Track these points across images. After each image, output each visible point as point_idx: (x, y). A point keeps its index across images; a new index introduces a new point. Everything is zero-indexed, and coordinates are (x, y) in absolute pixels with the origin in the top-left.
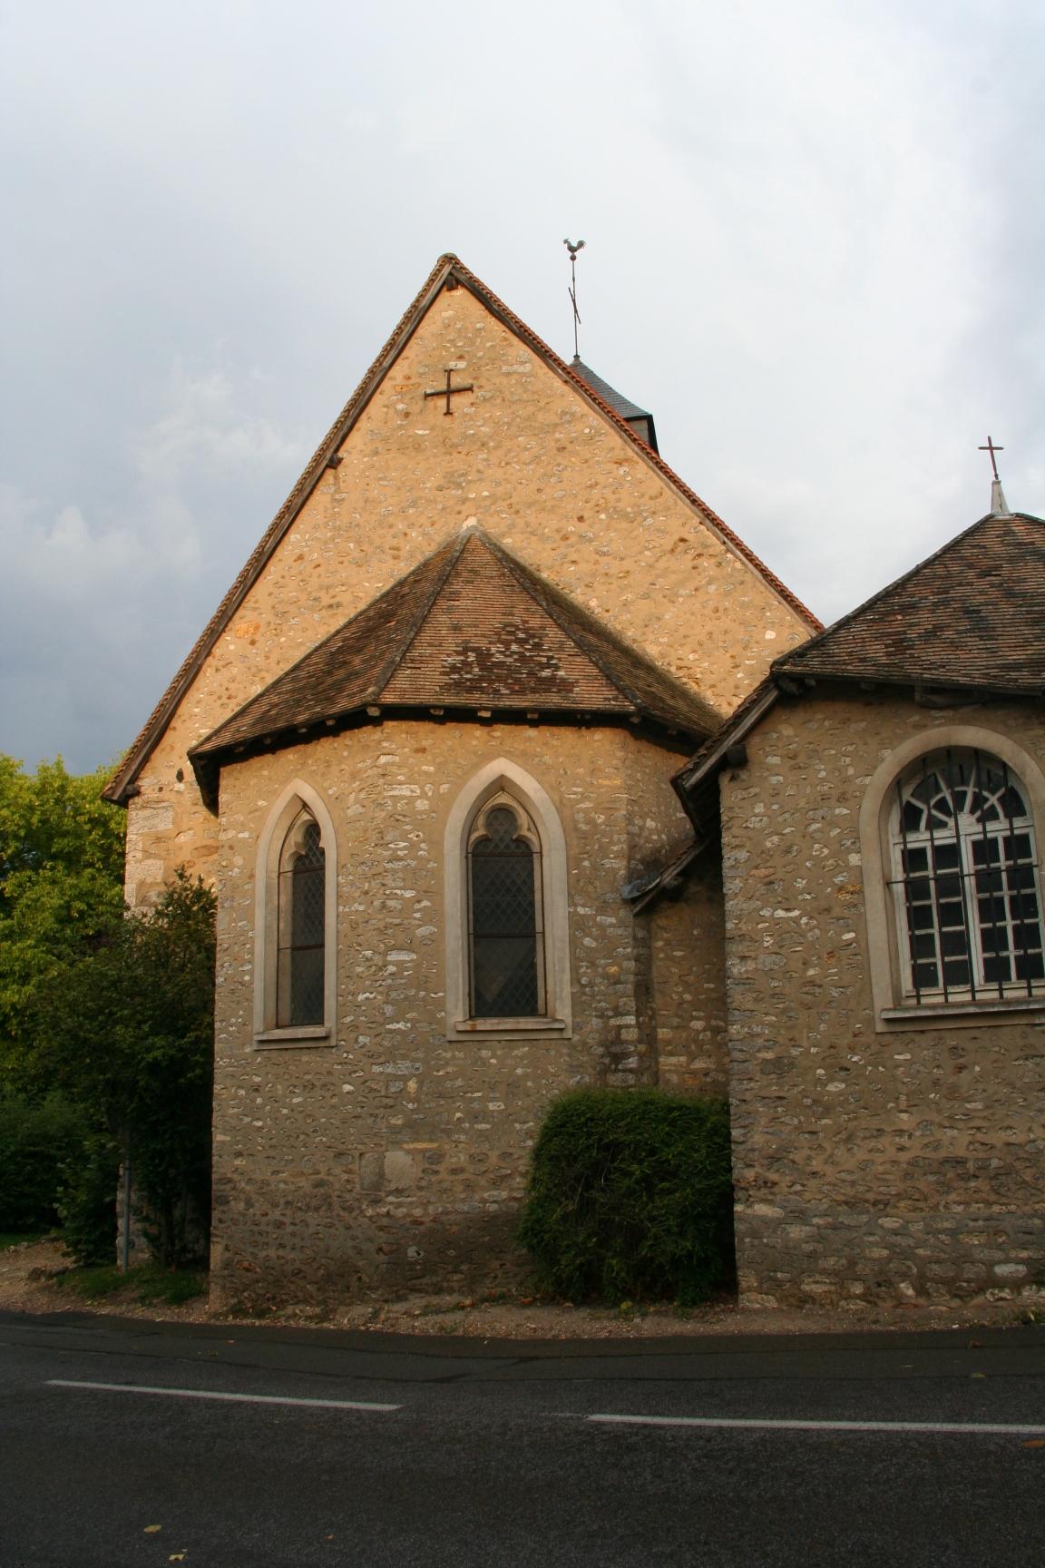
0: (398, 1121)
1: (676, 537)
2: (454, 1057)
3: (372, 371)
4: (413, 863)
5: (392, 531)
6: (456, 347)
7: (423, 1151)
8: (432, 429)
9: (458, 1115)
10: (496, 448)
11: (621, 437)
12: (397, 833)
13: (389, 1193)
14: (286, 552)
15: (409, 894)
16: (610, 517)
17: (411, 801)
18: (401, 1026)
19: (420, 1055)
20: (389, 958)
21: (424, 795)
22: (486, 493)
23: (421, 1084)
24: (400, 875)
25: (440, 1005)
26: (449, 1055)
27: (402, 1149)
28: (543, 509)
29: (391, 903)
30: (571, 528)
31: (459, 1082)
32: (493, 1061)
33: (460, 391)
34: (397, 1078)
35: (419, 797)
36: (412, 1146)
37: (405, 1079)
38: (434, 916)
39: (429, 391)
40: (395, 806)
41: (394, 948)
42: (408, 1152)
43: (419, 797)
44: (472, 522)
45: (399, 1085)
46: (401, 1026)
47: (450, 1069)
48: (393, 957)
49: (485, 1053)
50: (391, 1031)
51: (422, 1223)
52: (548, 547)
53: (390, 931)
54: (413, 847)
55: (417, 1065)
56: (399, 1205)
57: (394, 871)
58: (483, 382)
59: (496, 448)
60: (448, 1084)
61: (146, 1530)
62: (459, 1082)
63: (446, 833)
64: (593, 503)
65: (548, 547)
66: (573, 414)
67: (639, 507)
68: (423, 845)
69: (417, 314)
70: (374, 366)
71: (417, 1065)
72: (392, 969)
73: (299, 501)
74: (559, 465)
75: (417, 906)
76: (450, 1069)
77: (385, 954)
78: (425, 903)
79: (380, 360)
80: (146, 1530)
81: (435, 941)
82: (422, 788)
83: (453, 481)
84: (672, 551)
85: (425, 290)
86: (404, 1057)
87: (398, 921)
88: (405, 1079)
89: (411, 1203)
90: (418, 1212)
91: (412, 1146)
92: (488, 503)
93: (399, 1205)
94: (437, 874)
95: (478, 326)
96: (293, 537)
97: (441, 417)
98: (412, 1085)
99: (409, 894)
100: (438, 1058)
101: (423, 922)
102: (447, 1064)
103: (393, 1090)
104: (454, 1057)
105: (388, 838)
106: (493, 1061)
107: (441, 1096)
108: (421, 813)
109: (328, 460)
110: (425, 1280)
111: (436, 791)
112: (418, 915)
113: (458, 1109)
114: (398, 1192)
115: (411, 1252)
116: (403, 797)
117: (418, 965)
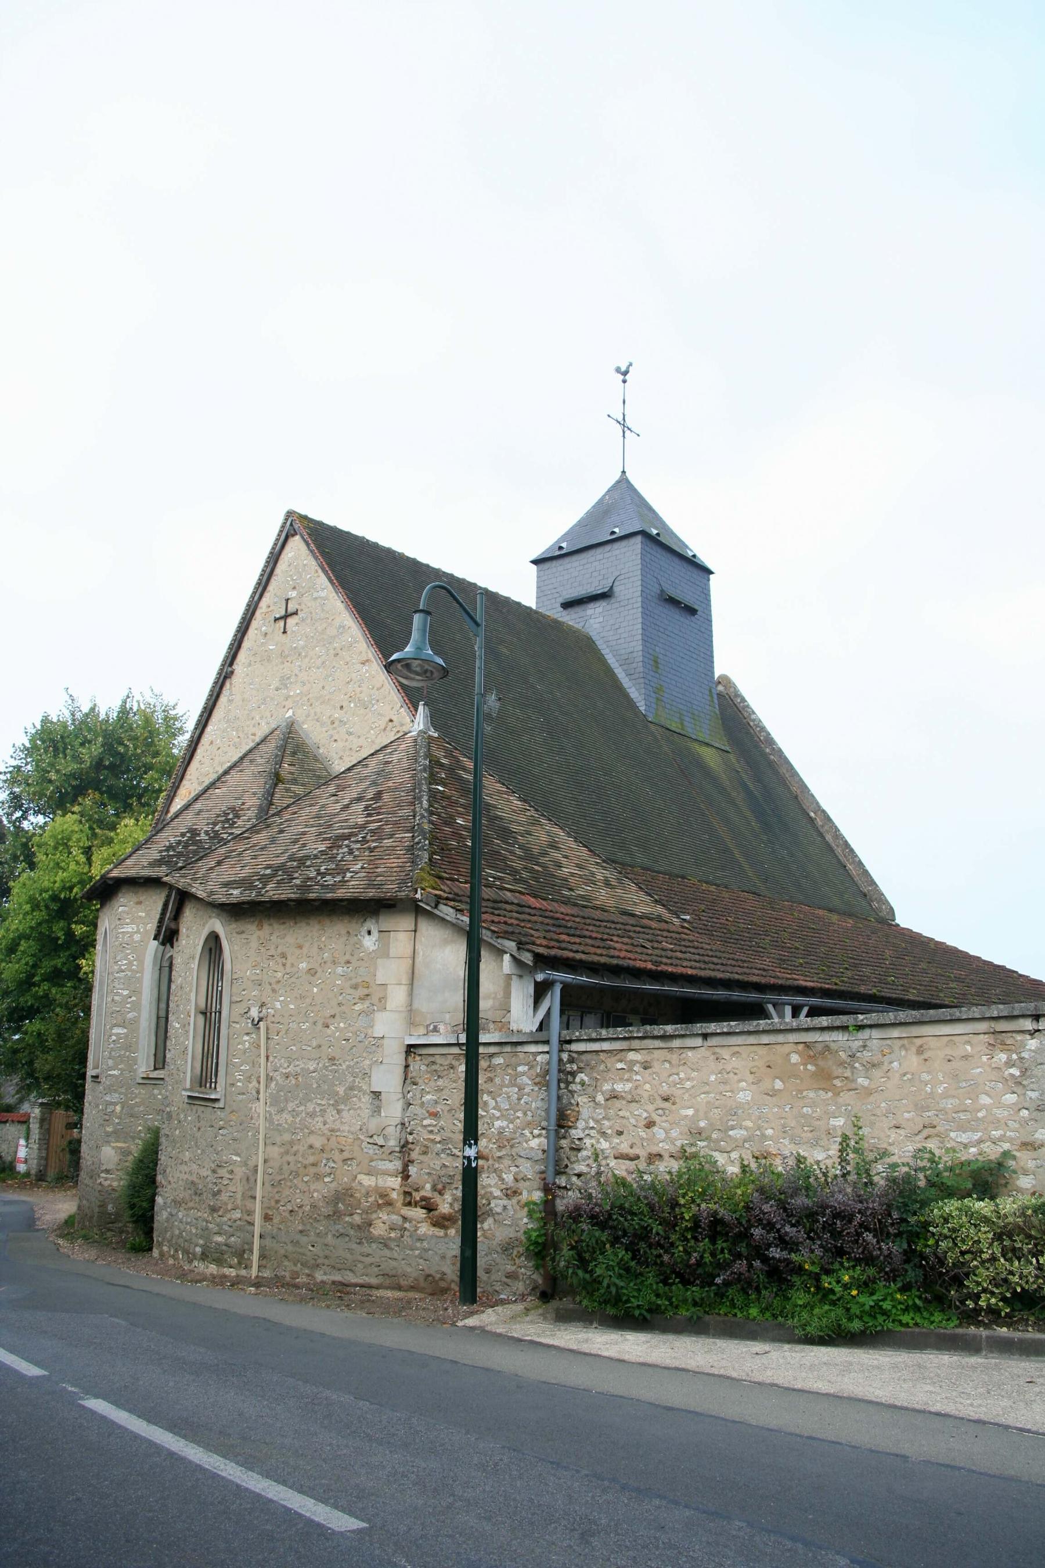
0: (109, 1129)
1: (387, 719)
2: (140, 1093)
3: (249, 605)
4: (129, 973)
5: (253, 722)
6: (293, 580)
7: (121, 1148)
8: (276, 645)
9: (140, 1128)
10: (306, 656)
11: (366, 643)
12: (122, 955)
13: (102, 1172)
14: (205, 740)
15: (126, 993)
16: (356, 706)
17: (131, 935)
18: (115, 1072)
19: (123, 1090)
20: (113, 1031)
21: (138, 932)
22: (298, 691)
23: (123, 1108)
24: (122, 981)
25: (135, 1060)
26: (137, 1091)
27: (110, 1146)
28: (324, 702)
29: (116, 998)
30: (337, 715)
31: (141, 1109)
32: (159, 1097)
33: (281, 618)
34: (112, 1103)
35: (136, 932)
36: (115, 1145)
37: (115, 1104)
38: (136, 1007)
39: (278, 616)
40: (123, 938)
41: (116, 1025)
42: (113, 1148)
43: (136, 932)
44: (290, 713)
45: (112, 1107)
46: (115, 1072)
47: (137, 1100)
48: (116, 1030)
49: (156, 1092)
50: (110, 1075)
51: (116, 1191)
52: (324, 729)
53: (114, 1015)
54: (130, 963)
55: (122, 1096)
56: (106, 1179)
57: (120, 978)
58: (303, 606)
59: (306, 656)
60: (136, 1109)
61: (46, 1373)
62: (141, 1109)
63: (147, 955)
64: (349, 695)
65: (324, 729)
66: (344, 627)
67: (371, 696)
68: (135, 963)
69: (274, 558)
70: (249, 601)
71: (122, 1096)
72: (114, 1038)
73: (211, 703)
74: (334, 667)
75: (129, 1000)
76: (137, 1100)
77: (111, 1029)
78: (133, 998)
79: (252, 597)
80: (46, 1373)
81: (136, 1021)
82: (138, 927)
83: (285, 682)
84: (385, 729)
85: (277, 540)
86: (115, 1091)
87: (118, 1009)
88: (115, 1104)
89: (112, 1178)
90: (115, 1184)
91: (115, 1145)
92: (298, 699)
93: (106, 1179)
94: (140, 980)
95: (305, 562)
96: (209, 728)
97: (281, 634)
98: (118, 1108)
99: (126, 993)
100: (132, 1093)
101: (132, 1010)
102: (136, 1097)
103: (108, 1110)
104: (140, 1093)
105: (118, 958)
106: (159, 1097)
107: (132, 1116)
108: (136, 942)
109: (224, 676)
110: (116, 1225)
111: (145, 929)
112: (128, 1006)
113: (140, 1125)
114: (107, 1171)
115: (110, 1207)
116: (128, 932)
117: (126, 1035)
